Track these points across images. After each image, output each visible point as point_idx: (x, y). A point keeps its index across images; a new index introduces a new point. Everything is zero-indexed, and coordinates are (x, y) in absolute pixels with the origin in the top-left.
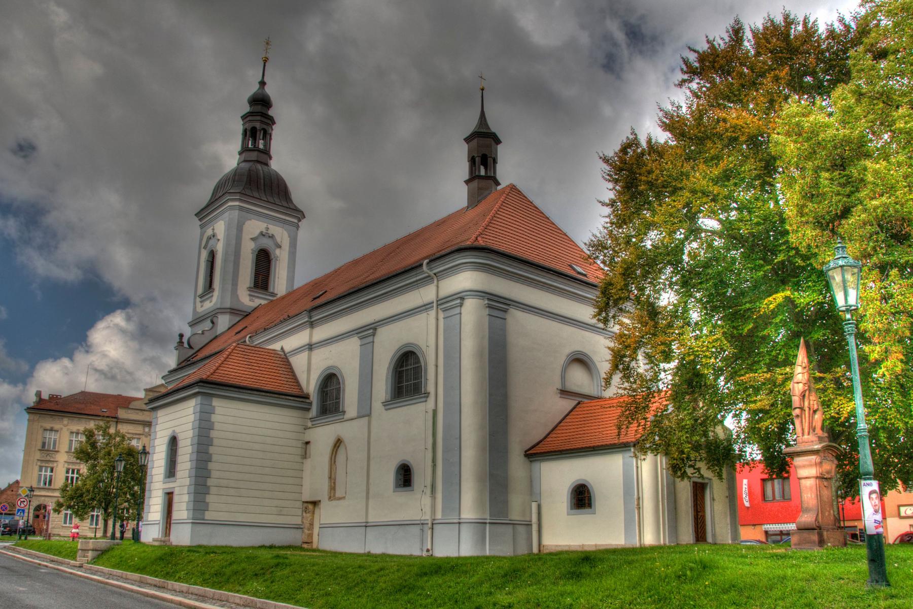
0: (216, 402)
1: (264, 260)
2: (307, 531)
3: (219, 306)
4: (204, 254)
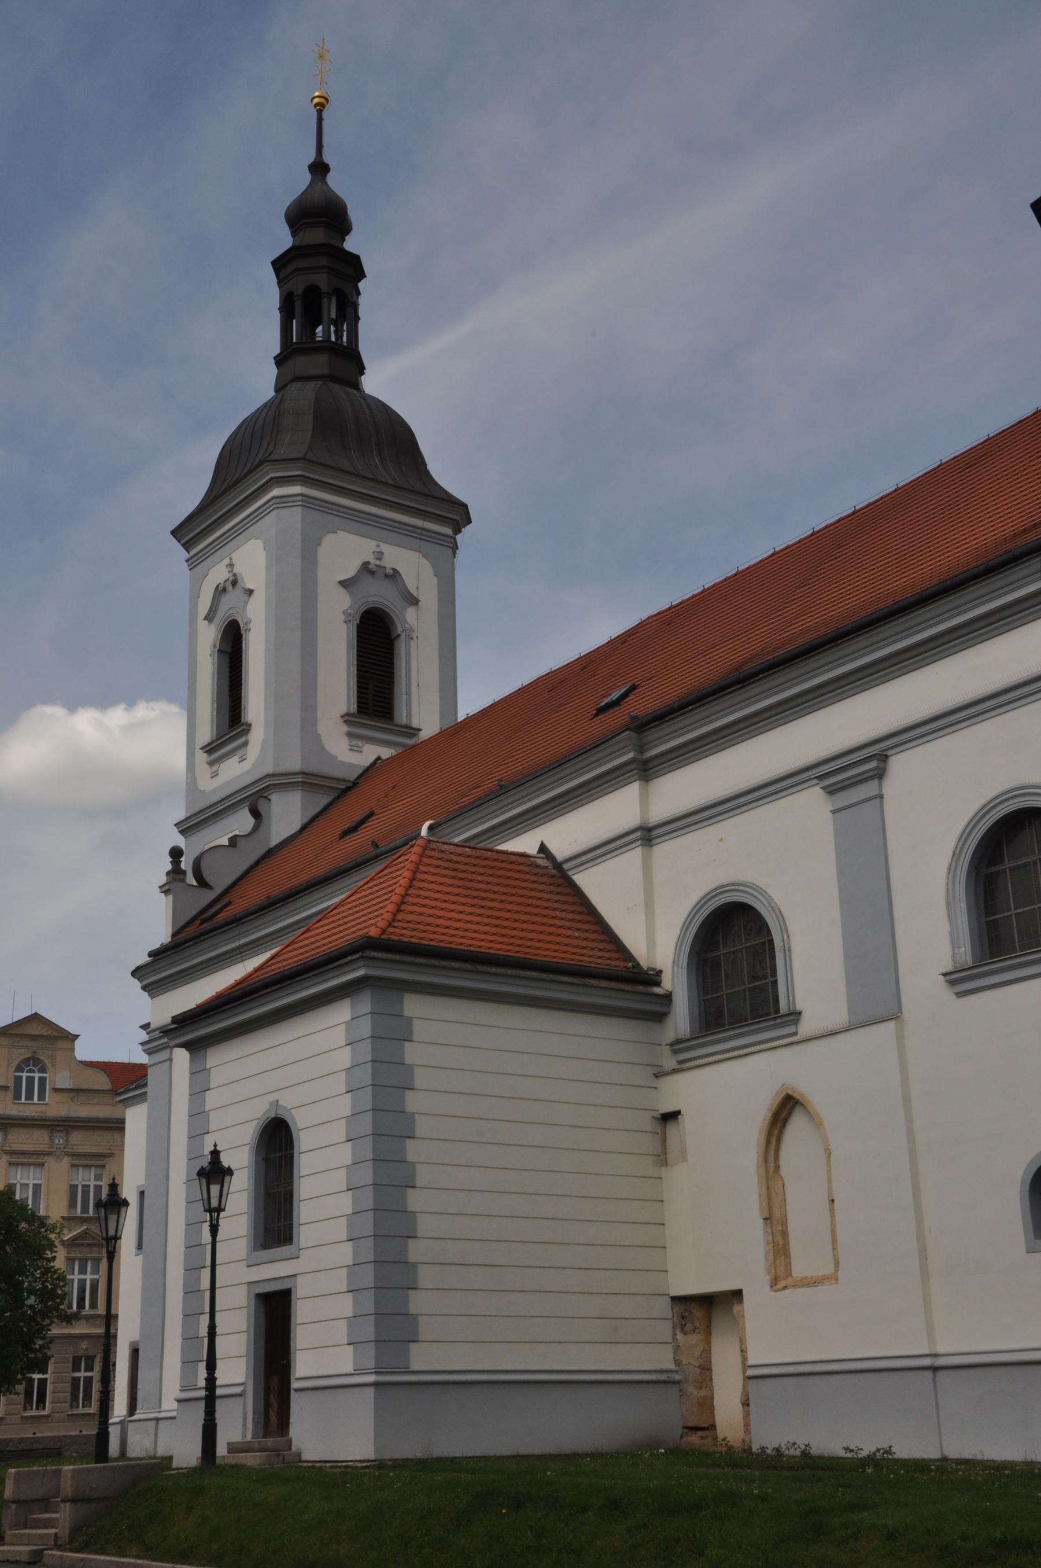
0: (413, 1005)
1: (376, 642)
2: (692, 1390)
3: (269, 770)
4: (209, 636)
